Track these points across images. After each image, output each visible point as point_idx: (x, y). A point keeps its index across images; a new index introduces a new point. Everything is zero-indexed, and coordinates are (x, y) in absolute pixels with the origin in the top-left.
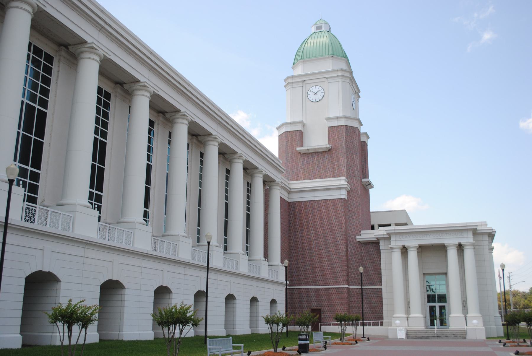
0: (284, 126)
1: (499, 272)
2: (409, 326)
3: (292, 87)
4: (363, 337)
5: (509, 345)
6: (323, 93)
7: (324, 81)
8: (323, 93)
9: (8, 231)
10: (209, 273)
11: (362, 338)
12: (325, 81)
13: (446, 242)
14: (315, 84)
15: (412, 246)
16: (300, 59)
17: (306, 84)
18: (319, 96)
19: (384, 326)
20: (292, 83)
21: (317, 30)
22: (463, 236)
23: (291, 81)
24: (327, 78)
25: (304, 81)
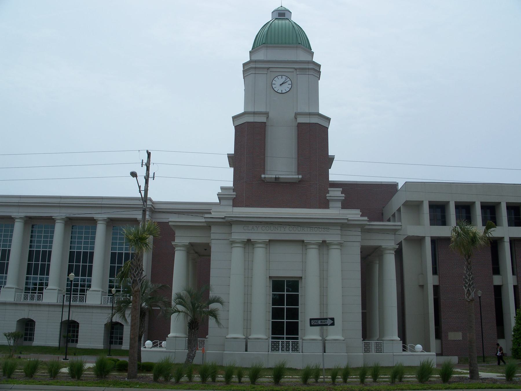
0: (246, 116)
1: (180, 250)
2: (326, 351)
3: (254, 72)
4: (65, 358)
5: (193, 336)
6: (290, 84)
7: (292, 71)
8: (290, 84)
9: (64, 307)
10: (64, 309)
11: (63, 359)
12: (293, 72)
13: (96, 216)
14: (282, 74)
15: (17, 217)
16: (264, 43)
17: (270, 71)
18: (286, 87)
19: (249, 352)
20: (255, 68)
21: (278, 17)
22: (327, 233)
23: (254, 66)
24: (296, 69)
25: (268, 68)
